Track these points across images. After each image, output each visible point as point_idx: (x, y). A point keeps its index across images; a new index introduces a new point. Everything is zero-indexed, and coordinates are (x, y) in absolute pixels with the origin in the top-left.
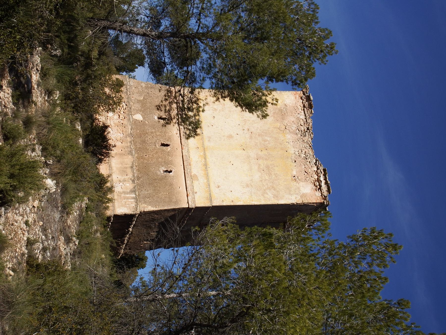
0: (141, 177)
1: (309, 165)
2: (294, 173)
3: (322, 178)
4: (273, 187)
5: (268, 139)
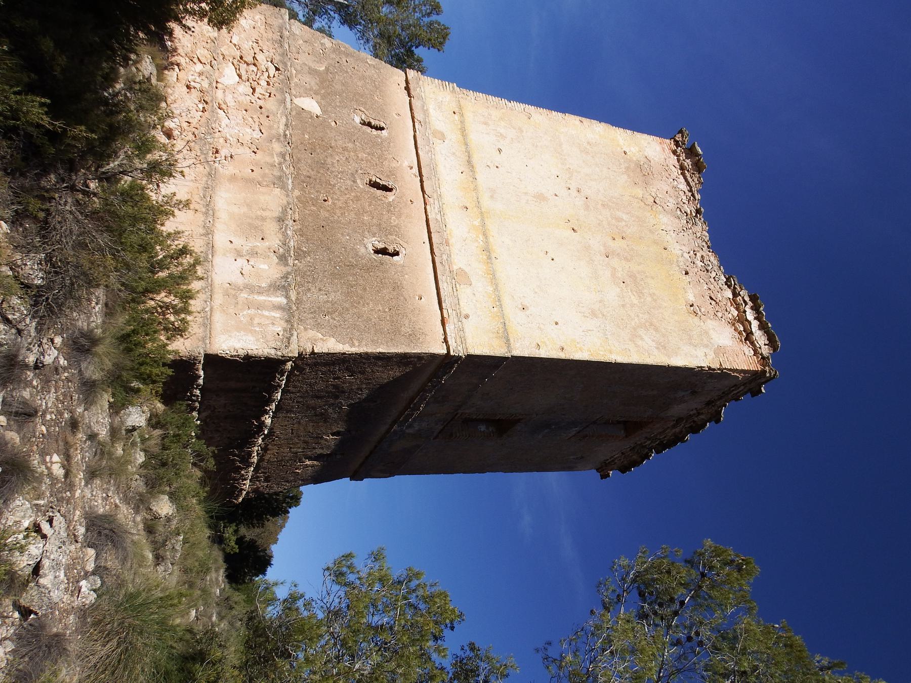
0: (308, 253)
1: (715, 283)
2: (691, 298)
3: (750, 315)
4: (651, 324)
5: (625, 217)
